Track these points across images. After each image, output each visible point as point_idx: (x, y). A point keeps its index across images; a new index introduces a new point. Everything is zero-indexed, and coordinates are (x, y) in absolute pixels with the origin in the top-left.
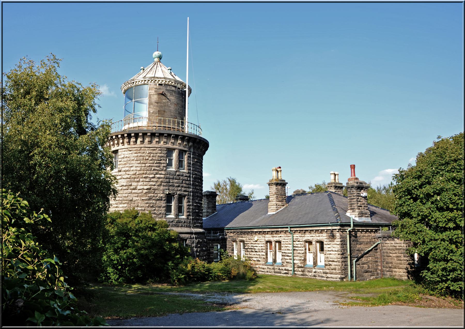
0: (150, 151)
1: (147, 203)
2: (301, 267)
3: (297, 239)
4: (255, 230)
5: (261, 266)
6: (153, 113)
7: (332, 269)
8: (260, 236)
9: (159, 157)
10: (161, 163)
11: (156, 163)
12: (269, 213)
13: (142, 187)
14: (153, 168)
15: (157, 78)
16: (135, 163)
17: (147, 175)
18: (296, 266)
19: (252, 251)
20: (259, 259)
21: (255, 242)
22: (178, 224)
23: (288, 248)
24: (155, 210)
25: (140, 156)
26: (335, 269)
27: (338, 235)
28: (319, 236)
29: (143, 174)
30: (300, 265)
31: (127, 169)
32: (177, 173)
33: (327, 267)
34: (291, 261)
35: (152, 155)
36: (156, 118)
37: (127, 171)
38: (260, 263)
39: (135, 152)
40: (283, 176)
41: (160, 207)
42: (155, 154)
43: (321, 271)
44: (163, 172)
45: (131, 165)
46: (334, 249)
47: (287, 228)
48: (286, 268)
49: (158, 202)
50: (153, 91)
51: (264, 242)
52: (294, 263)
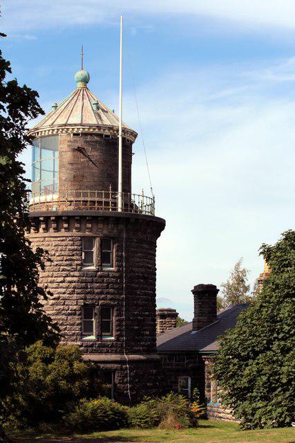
0: (57, 243)
6: (65, 180)
10: (74, 260)
11: (66, 260)
15: (70, 125)
17: (53, 279)
22: (101, 349)
29: (48, 276)
35: (60, 248)
41: (73, 325)
44: (77, 274)
49: (69, 318)
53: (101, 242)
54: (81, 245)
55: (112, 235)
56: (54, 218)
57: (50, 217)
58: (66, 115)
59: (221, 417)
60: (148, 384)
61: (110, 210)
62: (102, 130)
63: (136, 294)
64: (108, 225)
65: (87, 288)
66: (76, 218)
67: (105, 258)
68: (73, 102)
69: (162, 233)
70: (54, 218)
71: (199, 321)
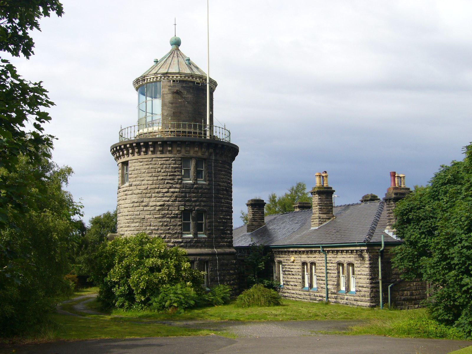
0: (162, 162)
1: (160, 222)
2: (334, 293)
3: (330, 260)
4: (291, 249)
5: (297, 292)
6: (167, 116)
7: (362, 296)
8: (296, 256)
9: (172, 168)
10: (176, 176)
11: (170, 176)
12: (312, 228)
13: (154, 203)
14: (166, 181)
15: (171, 73)
16: (146, 177)
17: (159, 190)
18: (329, 292)
19: (289, 274)
20: (296, 284)
21: (292, 264)
22: (197, 244)
23: (322, 270)
24: (169, 229)
25: (152, 168)
26: (364, 296)
27: (366, 256)
28: (350, 257)
29: (156, 188)
30: (333, 291)
31: (138, 183)
32: (195, 186)
33: (358, 293)
34: (325, 286)
35: (165, 166)
36: (170, 122)
37: (138, 185)
38: (297, 288)
39: (146, 163)
40: (329, 183)
41: (175, 226)
42: (168, 166)
43: (352, 297)
44: (178, 186)
45: (142, 179)
46: (363, 273)
47: (319, 247)
48: (321, 294)
49: (172, 220)
50: (167, 90)
51: (300, 264)
52: (327, 289)
53: (196, 162)
54: (181, 164)
55: (205, 157)
56: (160, 143)
57: (157, 142)
58: (166, 67)
59: (286, 296)
60: (231, 272)
61: (203, 138)
62: (194, 79)
63: (222, 203)
64: (202, 149)
65: (186, 197)
66: (178, 143)
67: (198, 174)
68: (170, 59)
69: (236, 158)
70: (160, 143)
71: (252, 225)
